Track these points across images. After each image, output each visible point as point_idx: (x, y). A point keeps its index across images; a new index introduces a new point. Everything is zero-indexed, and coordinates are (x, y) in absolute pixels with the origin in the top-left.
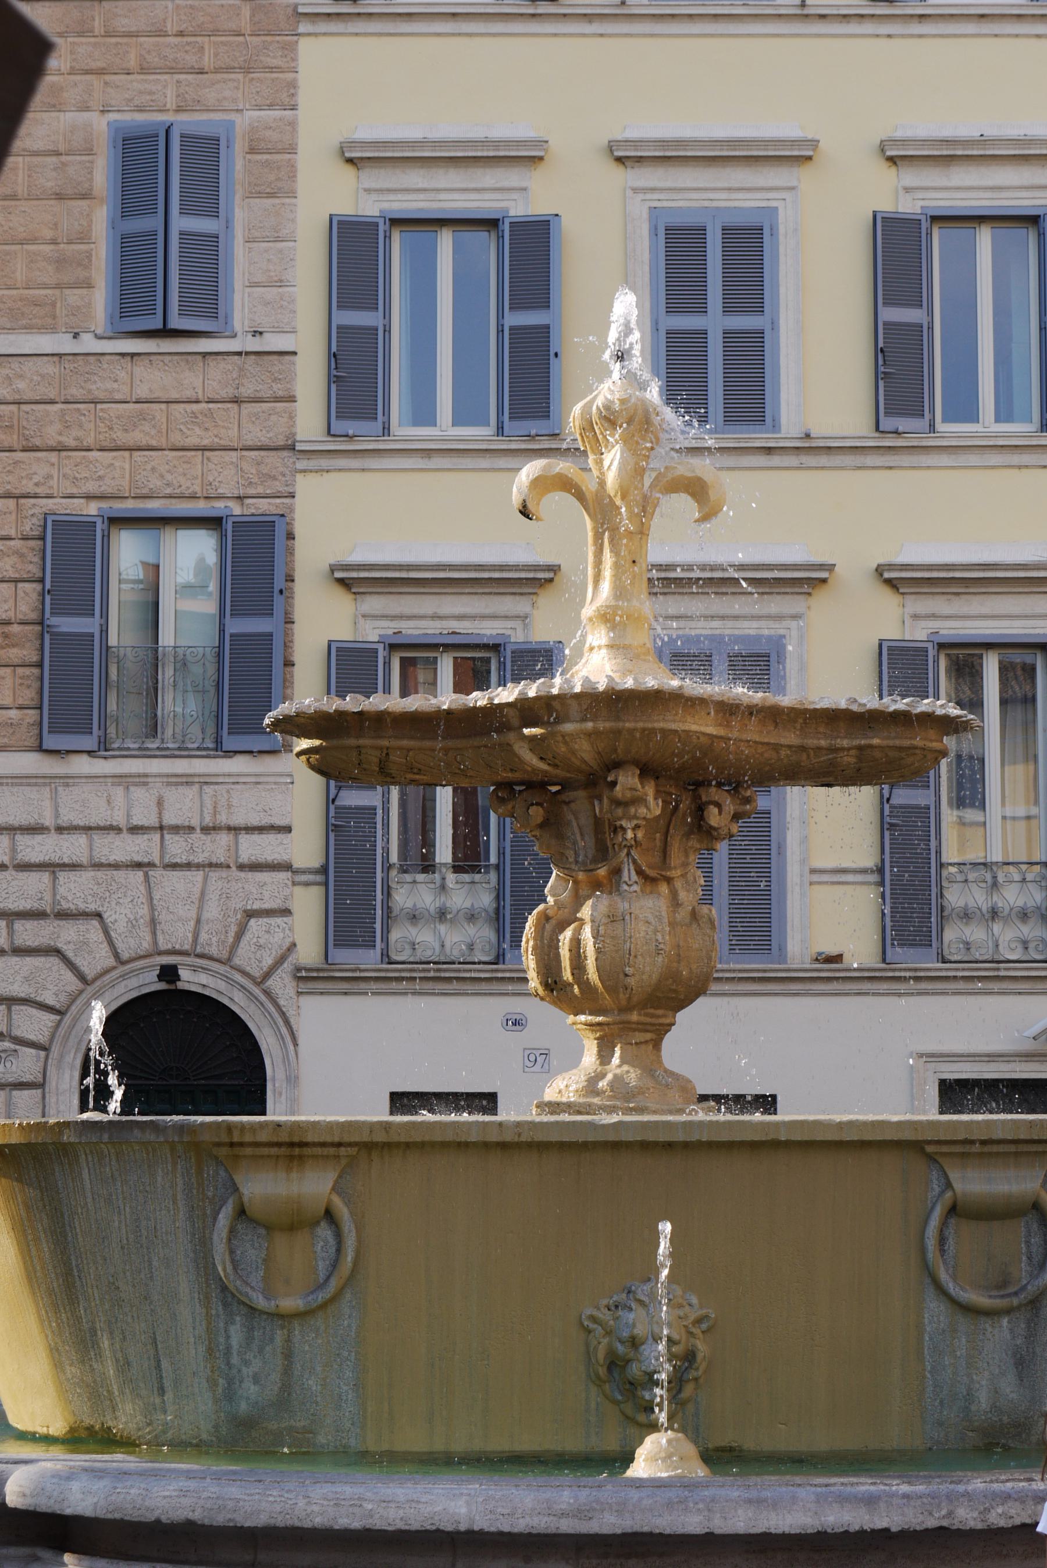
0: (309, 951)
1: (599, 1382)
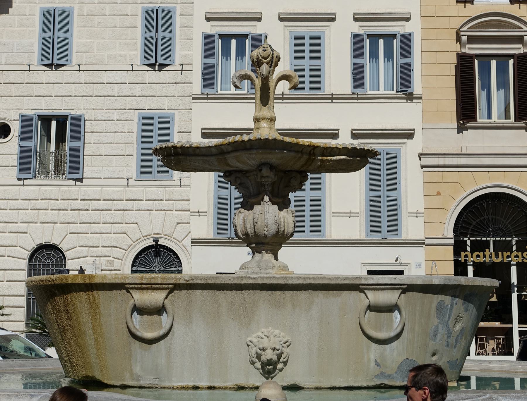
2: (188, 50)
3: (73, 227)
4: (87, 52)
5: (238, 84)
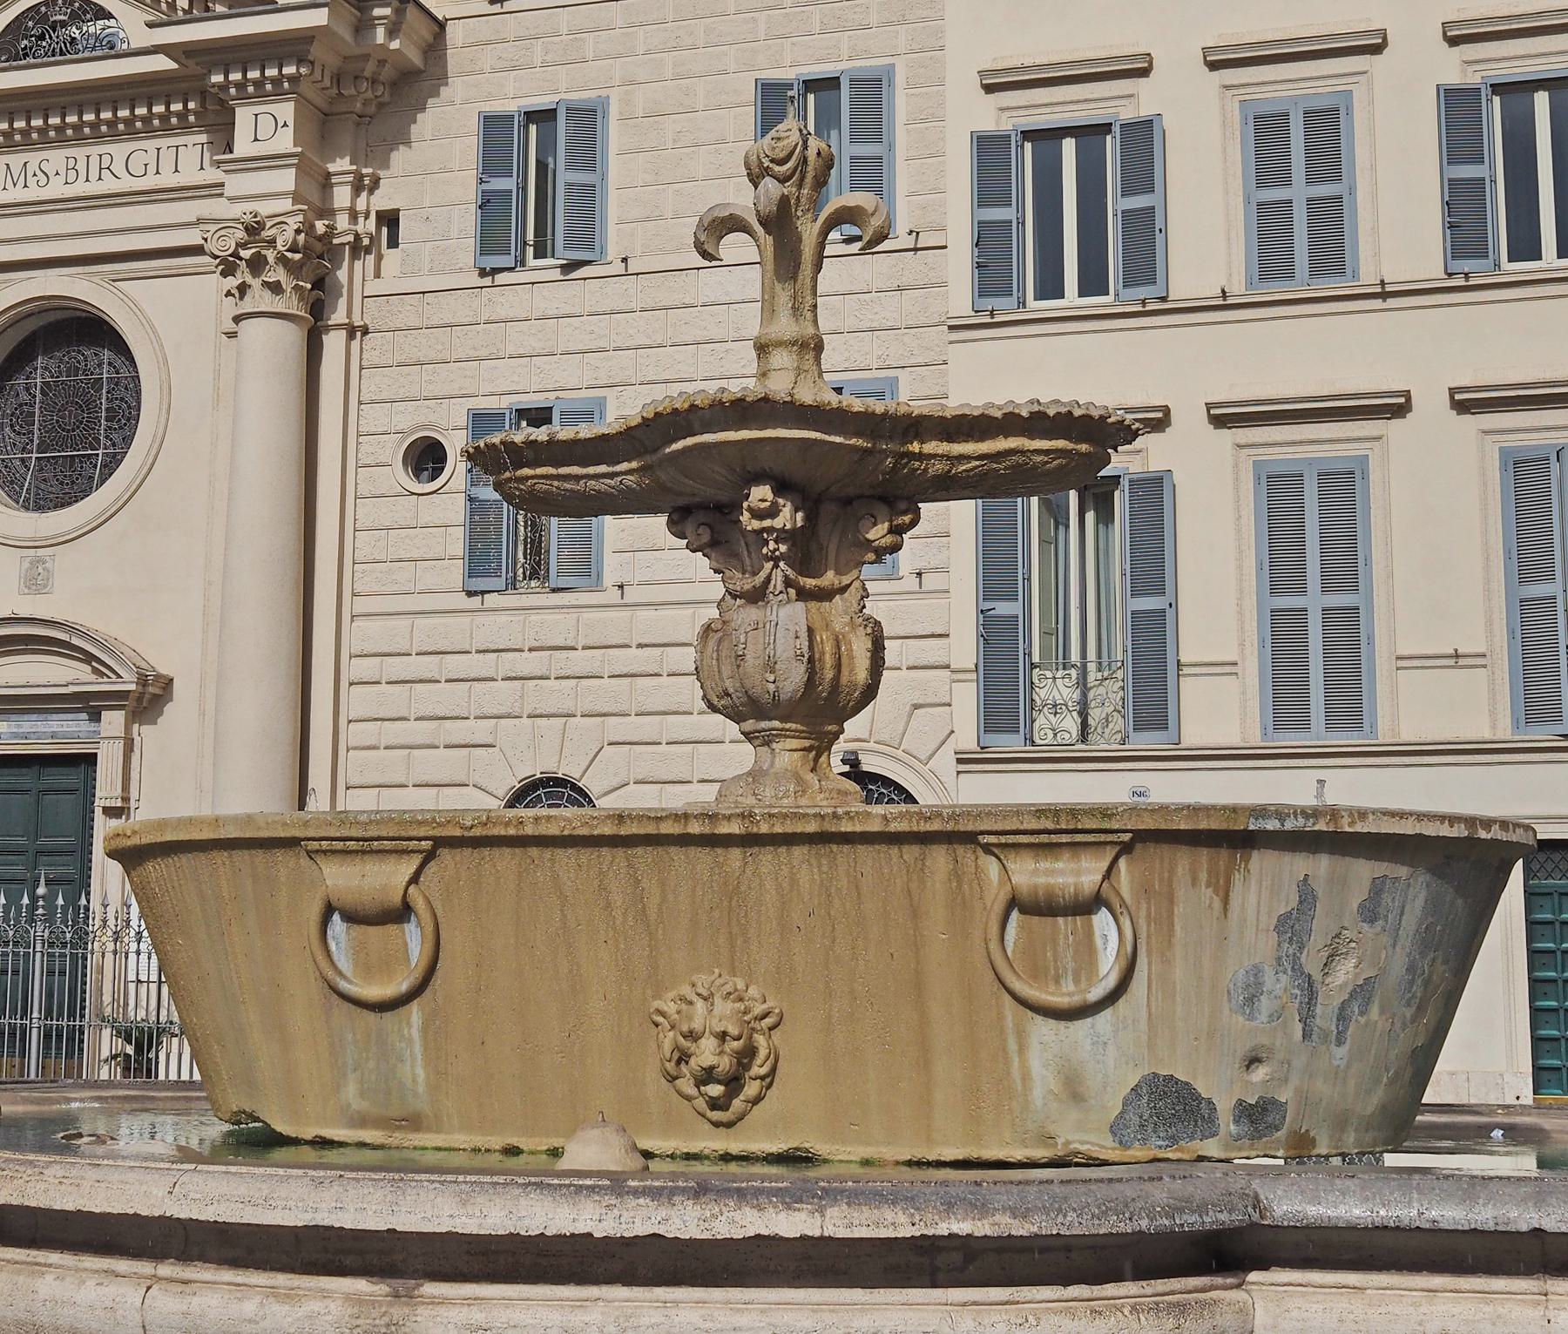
0: (967, 737)
2: (933, 188)
3: (617, 728)
4: (648, 219)
5: (709, 248)
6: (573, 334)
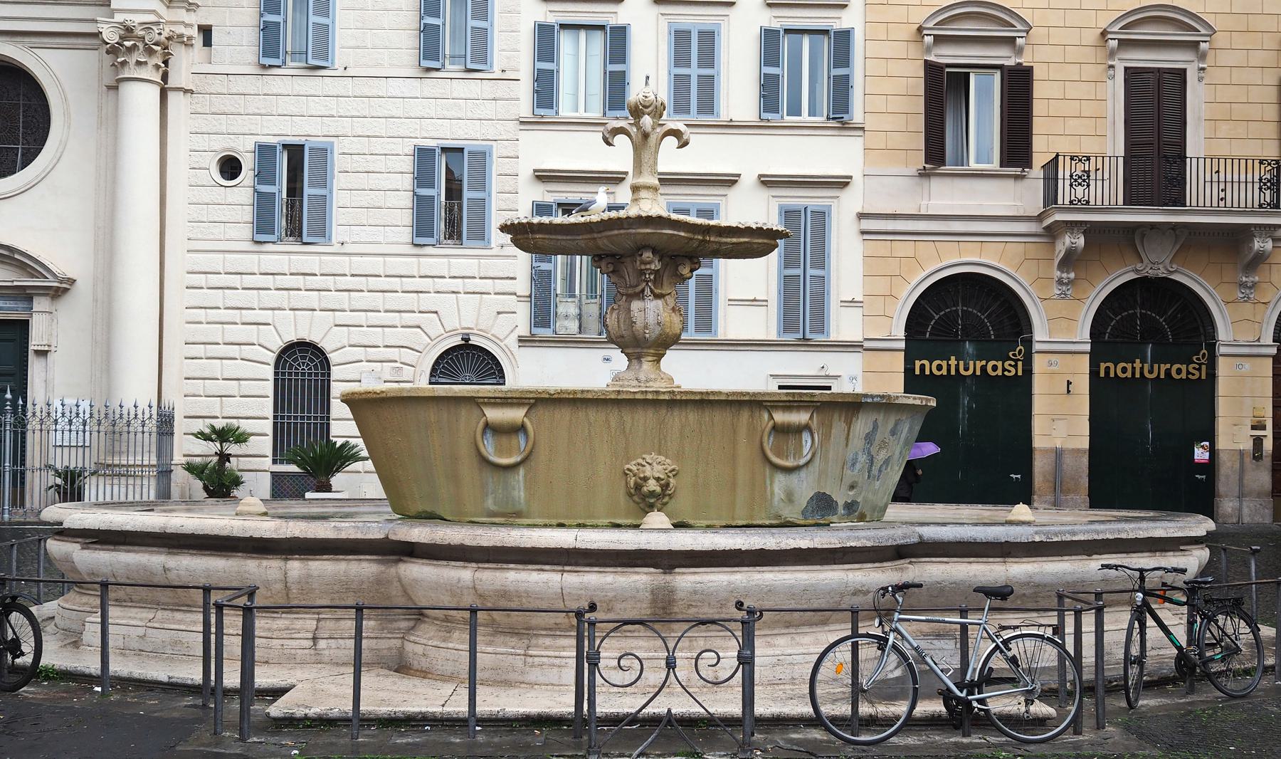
1: (630, 495)
6: (316, 106)
